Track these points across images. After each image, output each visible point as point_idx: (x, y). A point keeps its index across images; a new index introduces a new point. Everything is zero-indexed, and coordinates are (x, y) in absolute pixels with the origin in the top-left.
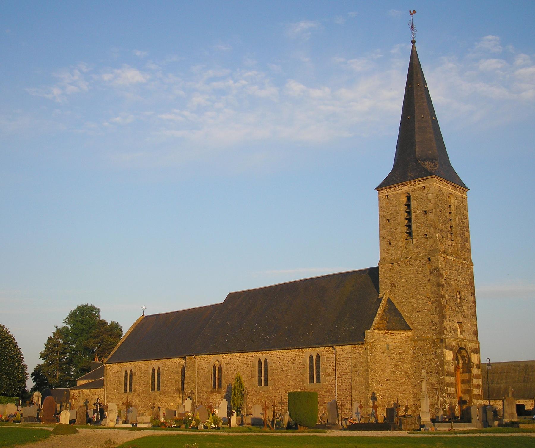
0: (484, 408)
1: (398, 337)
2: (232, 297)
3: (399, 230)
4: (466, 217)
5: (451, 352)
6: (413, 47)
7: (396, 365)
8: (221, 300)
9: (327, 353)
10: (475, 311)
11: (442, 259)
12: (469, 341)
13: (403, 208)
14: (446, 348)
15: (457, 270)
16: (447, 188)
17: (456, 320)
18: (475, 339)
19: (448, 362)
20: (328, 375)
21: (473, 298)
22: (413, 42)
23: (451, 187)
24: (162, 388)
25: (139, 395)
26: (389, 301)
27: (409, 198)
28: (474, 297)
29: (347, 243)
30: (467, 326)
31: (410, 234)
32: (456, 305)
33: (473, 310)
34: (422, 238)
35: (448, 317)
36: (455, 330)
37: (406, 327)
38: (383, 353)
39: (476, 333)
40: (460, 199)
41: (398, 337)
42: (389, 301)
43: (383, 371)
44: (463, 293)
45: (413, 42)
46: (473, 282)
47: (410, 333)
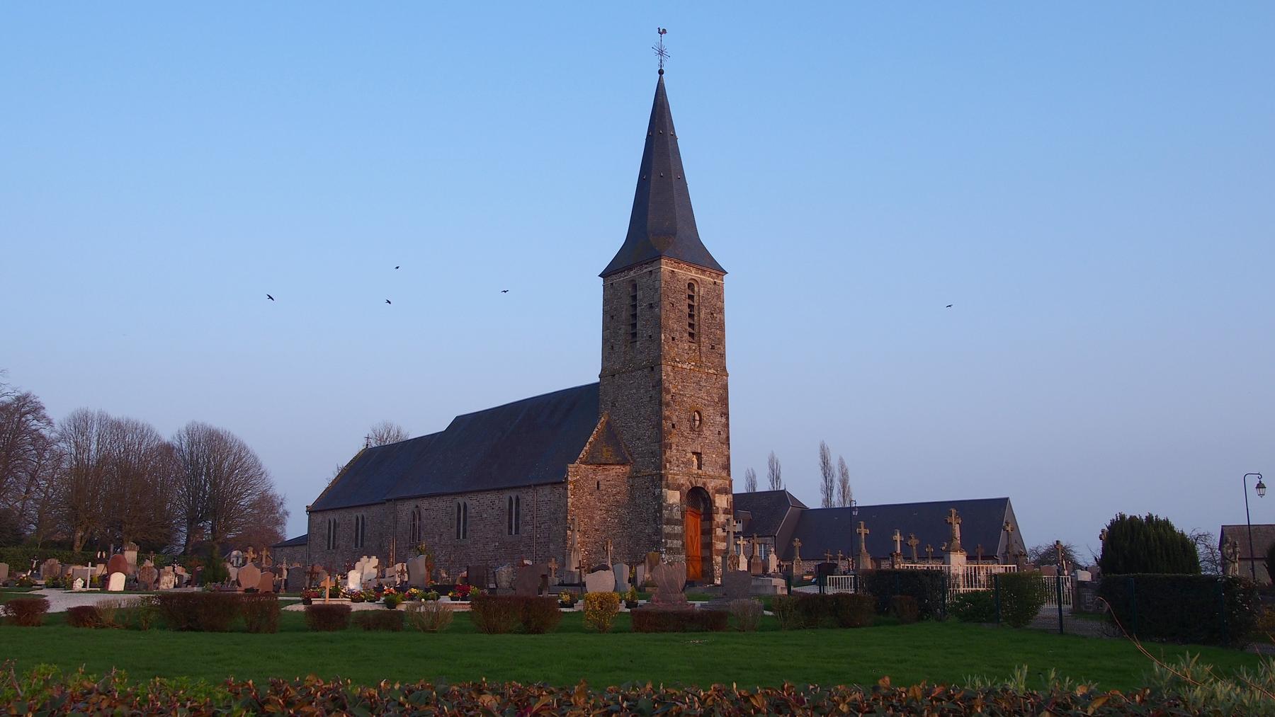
0: (331, 596)
1: (613, 473)
3: (622, 331)
4: (721, 311)
5: (678, 494)
6: (660, 80)
7: (607, 511)
8: (442, 426)
9: (528, 497)
10: (728, 438)
11: (669, 368)
12: (713, 477)
13: (628, 301)
14: (668, 487)
15: (698, 383)
16: (687, 273)
17: (689, 449)
18: (724, 474)
20: (527, 523)
21: (724, 420)
22: (661, 72)
24: (366, 544)
27: (635, 287)
29: (564, 350)
30: (710, 457)
31: (634, 335)
32: (692, 429)
33: (724, 436)
35: (674, 447)
36: (690, 462)
38: (591, 494)
39: (727, 467)
41: (613, 473)
44: (704, 414)
45: (661, 72)
46: (727, 398)
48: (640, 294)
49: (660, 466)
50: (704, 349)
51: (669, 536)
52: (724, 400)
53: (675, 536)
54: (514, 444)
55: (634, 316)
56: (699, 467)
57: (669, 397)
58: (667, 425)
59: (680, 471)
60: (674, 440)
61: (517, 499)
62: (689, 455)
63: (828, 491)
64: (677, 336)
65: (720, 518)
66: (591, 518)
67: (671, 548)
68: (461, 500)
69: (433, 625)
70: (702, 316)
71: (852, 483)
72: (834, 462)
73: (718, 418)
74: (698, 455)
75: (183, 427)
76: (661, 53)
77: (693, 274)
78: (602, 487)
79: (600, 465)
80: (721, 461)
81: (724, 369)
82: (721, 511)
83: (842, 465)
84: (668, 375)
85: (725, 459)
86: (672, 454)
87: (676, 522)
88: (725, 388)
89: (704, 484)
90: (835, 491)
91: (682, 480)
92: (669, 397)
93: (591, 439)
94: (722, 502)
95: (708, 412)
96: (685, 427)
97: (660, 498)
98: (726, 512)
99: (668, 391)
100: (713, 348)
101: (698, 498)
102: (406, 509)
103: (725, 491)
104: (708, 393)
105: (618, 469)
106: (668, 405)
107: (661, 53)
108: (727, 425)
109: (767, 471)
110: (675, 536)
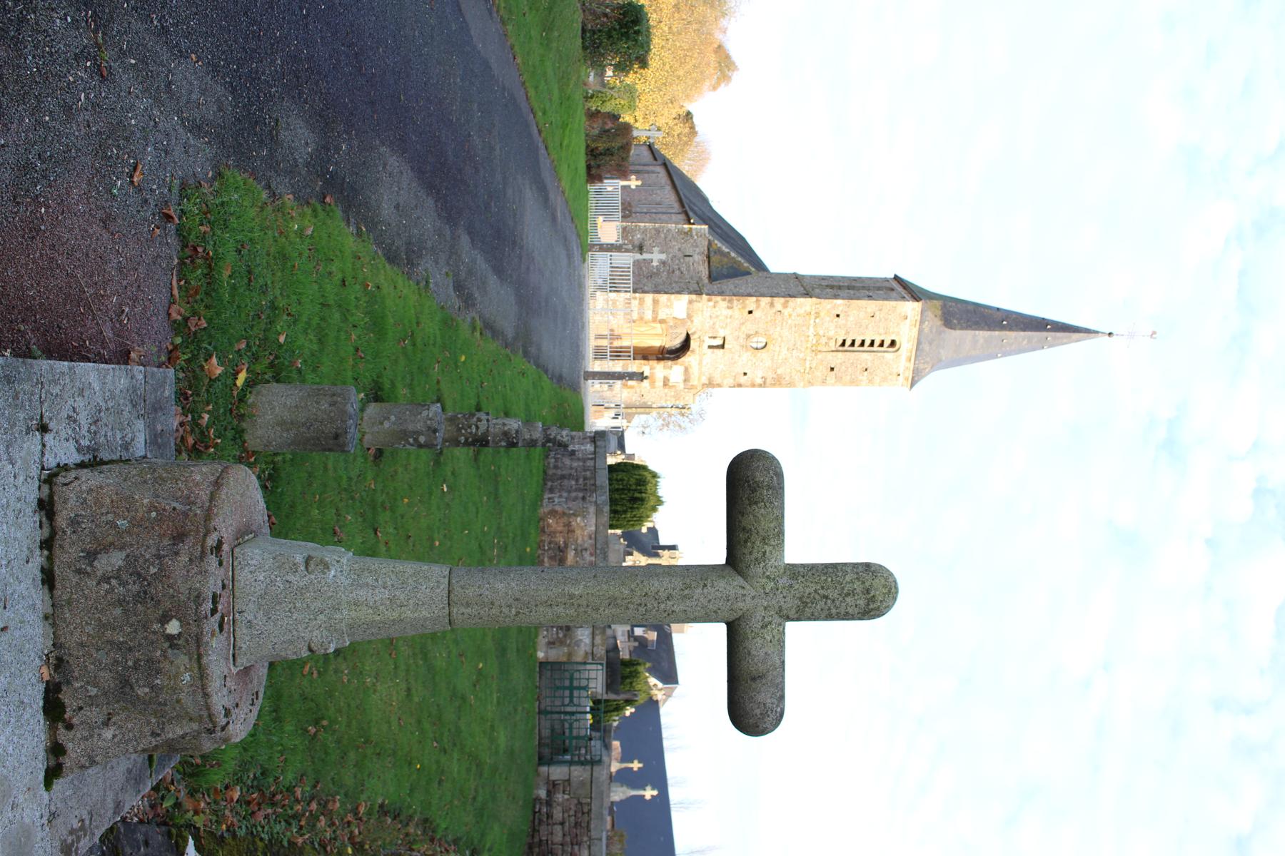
10: (740, 385)
11: (808, 309)
12: (700, 363)
14: (690, 302)
16: (907, 336)
26: (749, 273)
28: (760, 386)
32: (748, 336)
33: (743, 380)
35: (730, 312)
40: (895, 371)
42: (749, 273)
44: (763, 354)
47: (706, 281)
51: (642, 302)
52: (778, 382)
56: (710, 347)
58: (751, 302)
73: (760, 374)
79: (708, 257)
85: (719, 381)
93: (733, 254)
96: (749, 328)
100: (832, 369)
106: (772, 305)
108: (753, 386)
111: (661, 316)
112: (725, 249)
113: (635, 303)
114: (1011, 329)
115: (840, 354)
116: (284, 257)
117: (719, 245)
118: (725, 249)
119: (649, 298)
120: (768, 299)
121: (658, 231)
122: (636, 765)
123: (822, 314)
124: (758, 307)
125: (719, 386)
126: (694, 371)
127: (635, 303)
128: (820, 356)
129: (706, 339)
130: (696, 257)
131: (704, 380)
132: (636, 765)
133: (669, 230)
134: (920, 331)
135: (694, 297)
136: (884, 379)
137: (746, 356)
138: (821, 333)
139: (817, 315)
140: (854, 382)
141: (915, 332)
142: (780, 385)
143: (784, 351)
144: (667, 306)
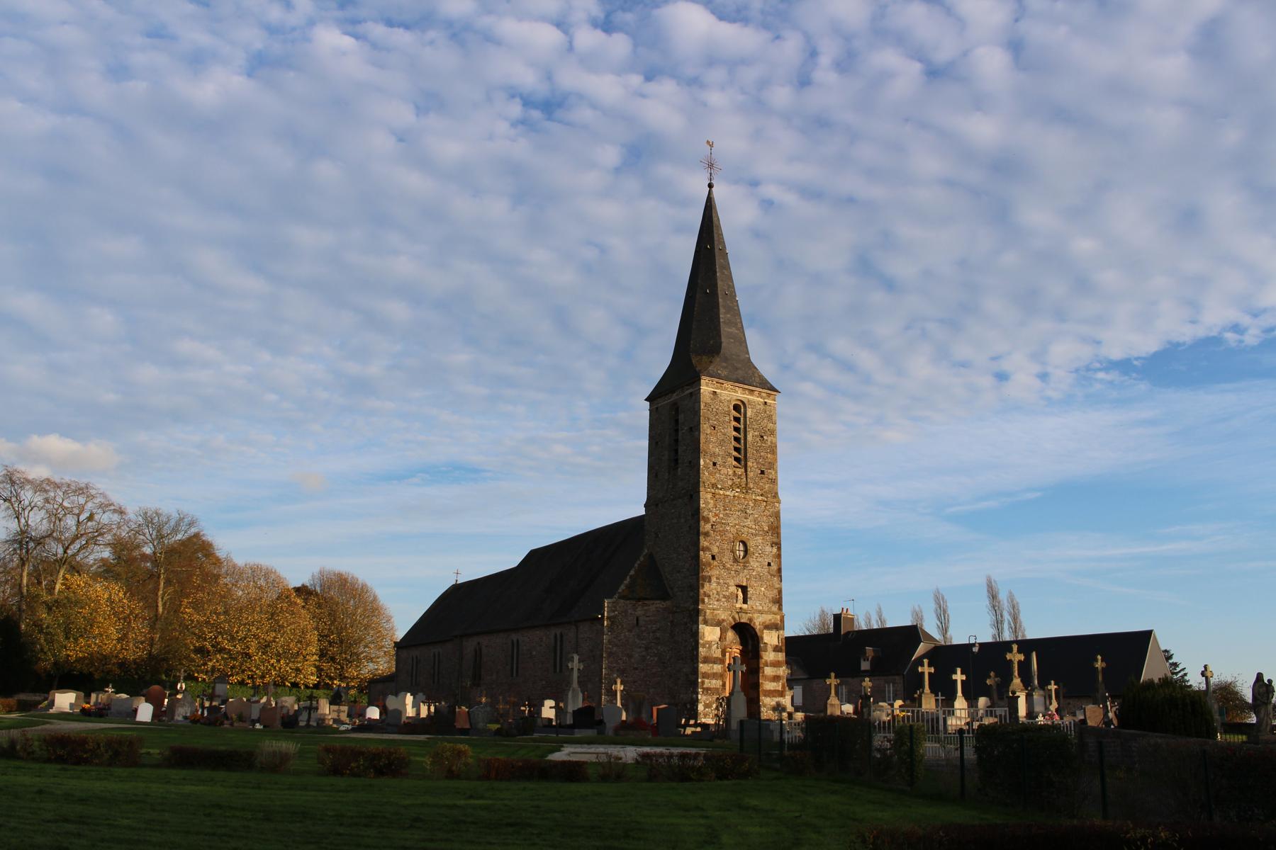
1: (653, 608)
2: (537, 558)
6: (710, 193)
7: (647, 649)
8: (510, 559)
10: (779, 570)
11: (709, 496)
12: (761, 612)
14: (706, 623)
16: (731, 393)
19: (710, 643)
21: (775, 550)
22: (710, 186)
23: (740, 391)
25: (342, 642)
26: (651, 556)
28: (779, 549)
31: (676, 460)
32: (736, 560)
33: (774, 567)
34: (54, 655)
35: (714, 579)
37: (664, 596)
38: (630, 631)
39: (778, 601)
40: (762, 407)
41: (653, 608)
42: (651, 556)
43: (630, 656)
44: (751, 544)
45: (710, 186)
47: (668, 603)
48: (681, 417)
49: (696, 600)
50: (751, 475)
51: (706, 675)
52: (775, 529)
53: (714, 676)
54: (566, 578)
55: (677, 441)
56: (745, 601)
57: (708, 527)
58: (705, 557)
59: (718, 602)
60: (715, 572)
61: (561, 636)
62: (733, 589)
63: (998, 624)
64: (719, 461)
65: (769, 656)
66: (630, 656)
67: (708, 689)
68: (514, 637)
69: (278, 764)
70: (749, 438)
71: (1023, 617)
72: (1003, 596)
73: (768, 549)
74: (744, 589)
75: (316, 570)
76: (711, 166)
77: (739, 394)
78: (641, 622)
79: (639, 600)
80: (772, 594)
81: (776, 495)
82: (770, 648)
83: (1011, 598)
84: (707, 503)
85: (776, 592)
86: (710, 588)
87: (715, 661)
88: (777, 515)
89: (750, 620)
90: (1006, 626)
91: (723, 615)
92: (708, 527)
93: (632, 572)
94: (770, 638)
95: (755, 542)
96: (727, 559)
97: (695, 635)
98: (776, 649)
99: (707, 520)
100: (762, 472)
101: (747, 634)
102: (470, 645)
103: (777, 627)
104: (756, 521)
105: (659, 604)
106: (707, 534)
107: (711, 166)
108: (779, 556)
109: (933, 605)
110: (714, 676)
111: (718, 654)
112: (627, 581)
113: (708, 683)
114: (716, 285)
115: (749, 464)
116: (40, 792)
117: (623, 587)
118: (627, 581)
119: (703, 668)
120: (702, 538)
121: (610, 654)
122: (959, 677)
123: (713, 481)
124: (708, 549)
125: (780, 592)
126: (768, 618)
127: (708, 683)
128: (751, 485)
129: (738, 605)
130: (639, 612)
131: (775, 608)
132: (959, 677)
133: (610, 642)
134: (727, 379)
135: (701, 618)
136: (770, 418)
137: (753, 563)
138: (730, 483)
139: (714, 486)
140: (773, 450)
141: (727, 385)
142: (778, 527)
143: (749, 522)
144: (710, 647)
